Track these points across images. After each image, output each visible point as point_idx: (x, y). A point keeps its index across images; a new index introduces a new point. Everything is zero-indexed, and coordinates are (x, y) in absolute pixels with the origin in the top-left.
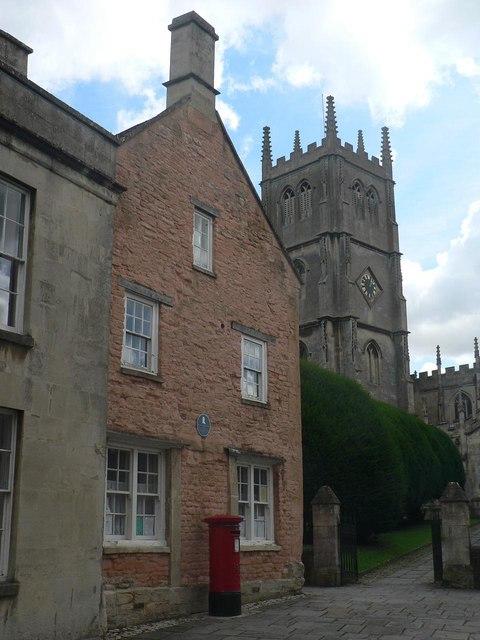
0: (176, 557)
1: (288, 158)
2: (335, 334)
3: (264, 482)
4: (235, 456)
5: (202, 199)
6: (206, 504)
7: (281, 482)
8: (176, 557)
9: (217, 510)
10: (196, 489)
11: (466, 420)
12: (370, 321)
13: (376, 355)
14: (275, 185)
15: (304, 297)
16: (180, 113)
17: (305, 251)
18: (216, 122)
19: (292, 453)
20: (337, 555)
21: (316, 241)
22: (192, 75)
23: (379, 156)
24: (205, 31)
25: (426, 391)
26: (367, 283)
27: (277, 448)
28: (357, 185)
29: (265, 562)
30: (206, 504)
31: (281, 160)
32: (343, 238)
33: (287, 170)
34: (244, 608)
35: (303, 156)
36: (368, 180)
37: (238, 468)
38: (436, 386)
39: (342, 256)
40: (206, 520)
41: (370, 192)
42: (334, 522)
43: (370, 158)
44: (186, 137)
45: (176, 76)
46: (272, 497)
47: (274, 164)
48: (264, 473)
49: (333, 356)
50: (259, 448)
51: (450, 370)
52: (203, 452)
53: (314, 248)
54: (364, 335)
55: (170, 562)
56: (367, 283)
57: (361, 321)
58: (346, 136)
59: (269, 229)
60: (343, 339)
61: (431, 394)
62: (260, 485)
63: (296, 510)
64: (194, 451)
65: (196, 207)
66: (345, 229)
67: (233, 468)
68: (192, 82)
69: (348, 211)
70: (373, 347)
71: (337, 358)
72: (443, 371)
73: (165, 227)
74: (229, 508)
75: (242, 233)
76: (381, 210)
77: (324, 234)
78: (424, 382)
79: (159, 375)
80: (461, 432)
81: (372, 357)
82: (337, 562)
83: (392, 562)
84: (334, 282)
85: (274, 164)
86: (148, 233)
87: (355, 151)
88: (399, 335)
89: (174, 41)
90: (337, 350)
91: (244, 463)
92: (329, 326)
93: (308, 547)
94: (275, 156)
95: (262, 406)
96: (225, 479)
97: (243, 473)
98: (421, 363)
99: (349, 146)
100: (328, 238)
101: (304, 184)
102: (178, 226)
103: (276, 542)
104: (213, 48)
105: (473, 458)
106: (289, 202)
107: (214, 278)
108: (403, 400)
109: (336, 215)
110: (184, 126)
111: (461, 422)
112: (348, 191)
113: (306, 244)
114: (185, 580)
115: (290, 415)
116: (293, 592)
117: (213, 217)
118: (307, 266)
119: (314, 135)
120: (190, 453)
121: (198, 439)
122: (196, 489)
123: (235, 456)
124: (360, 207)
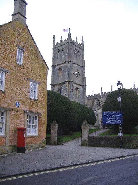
0: (8, 138)
1: (59, 43)
2: (68, 85)
3: (36, 119)
4: (27, 113)
5: (20, 45)
6: (17, 125)
7: (40, 119)
8: (8, 138)
9: (21, 126)
10: (15, 121)
11: (98, 106)
12: (77, 82)
13: (78, 90)
14: (56, 49)
15: (62, 76)
16: (14, 23)
17: (62, 65)
18: (26, 26)
19: (44, 112)
20: (56, 138)
21: (65, 63)
22: (19, 13)
23: (81, 43)
24: (23, 2)
25: (90, 99)
26: (77, 73)
27: (40, 111)
28: (75, 50)
29: (35, 139)
30: (17, 125)
31: (57, 43)
32: (71, 62)
33: (59, 46)
34: (26, 152)
35: (63, 42)
36: (78, 49)
37: (28, 116)
38: (92, 98)
39: (71, 66)
40: (17, 129)
41: (78, 52)
42: (56, 130)
43: (79, 44)
44: (16, 29)
45: (15, 13)
46: (38, 123)
47: (56, 44)
48: (36, 117)
49: (68, 90)
50: (34, 111)
51: (95, 95)
52: (17, 111)
53: (64, 65)
54: (76, 86)
55: (6, 139)
56: (77, 73)
57: (75, 82)
58: (73, 38)
59: (40, 55)
60: (70, 86)
61: (91, 100)
62: (34, 120)
63: (44, 127)
64: (14, 111)
65: (18, 48)
66: (72, 61)
67: (26, 116)
68: (19, 15)
69: (73, 56)
70: (78, 88)
71: (69, 91)
72: (94, 95)
73: (8, 52)
74: (24, 126)
75: (32, 56)
76: (81, 56)
77: (67, 61)
78: (89, 97)
79: (5, 91)
80: (97, 109)
81: (77, 91)
82: (56, 139)
83: (73, 139)
84: (69, 73)
85: (56, 44)
86: (3, 53)
87: (75, 42)
88: (84, 86)
89: (15, 4)
90: (69, 89)
91: (29, 115)
92: (67, 83)
93: (48, 136)
94: (56, 42)
95: (35, 100)
96: (24, 118)
97: (29, 117)
98: (118, 101)
99: (80, 44)
100: (68, 62)
101: (63, 49)
102: (12, 52)
103: (39, 134)
104: (26, 7)
105: (99, 115)
106: (59, 54)
107: (23, 66)
108: (84, 102)
109: (70, 57)
110: (16, 27)
111: (97, 107)
112: (73, 51)
113: (63, 64)
114: (10, 144)
115: (44, 103)
116: (42, 147)
117: (24, 51)
118: (63, 69)
119: (65, 37)
120: (13, 112)
121: (16, 108)
122: (15, 121)
123: (27, 113)
124: (76, 55)
